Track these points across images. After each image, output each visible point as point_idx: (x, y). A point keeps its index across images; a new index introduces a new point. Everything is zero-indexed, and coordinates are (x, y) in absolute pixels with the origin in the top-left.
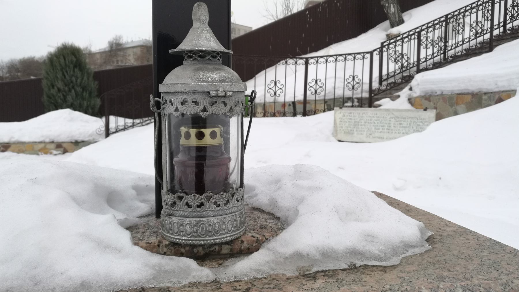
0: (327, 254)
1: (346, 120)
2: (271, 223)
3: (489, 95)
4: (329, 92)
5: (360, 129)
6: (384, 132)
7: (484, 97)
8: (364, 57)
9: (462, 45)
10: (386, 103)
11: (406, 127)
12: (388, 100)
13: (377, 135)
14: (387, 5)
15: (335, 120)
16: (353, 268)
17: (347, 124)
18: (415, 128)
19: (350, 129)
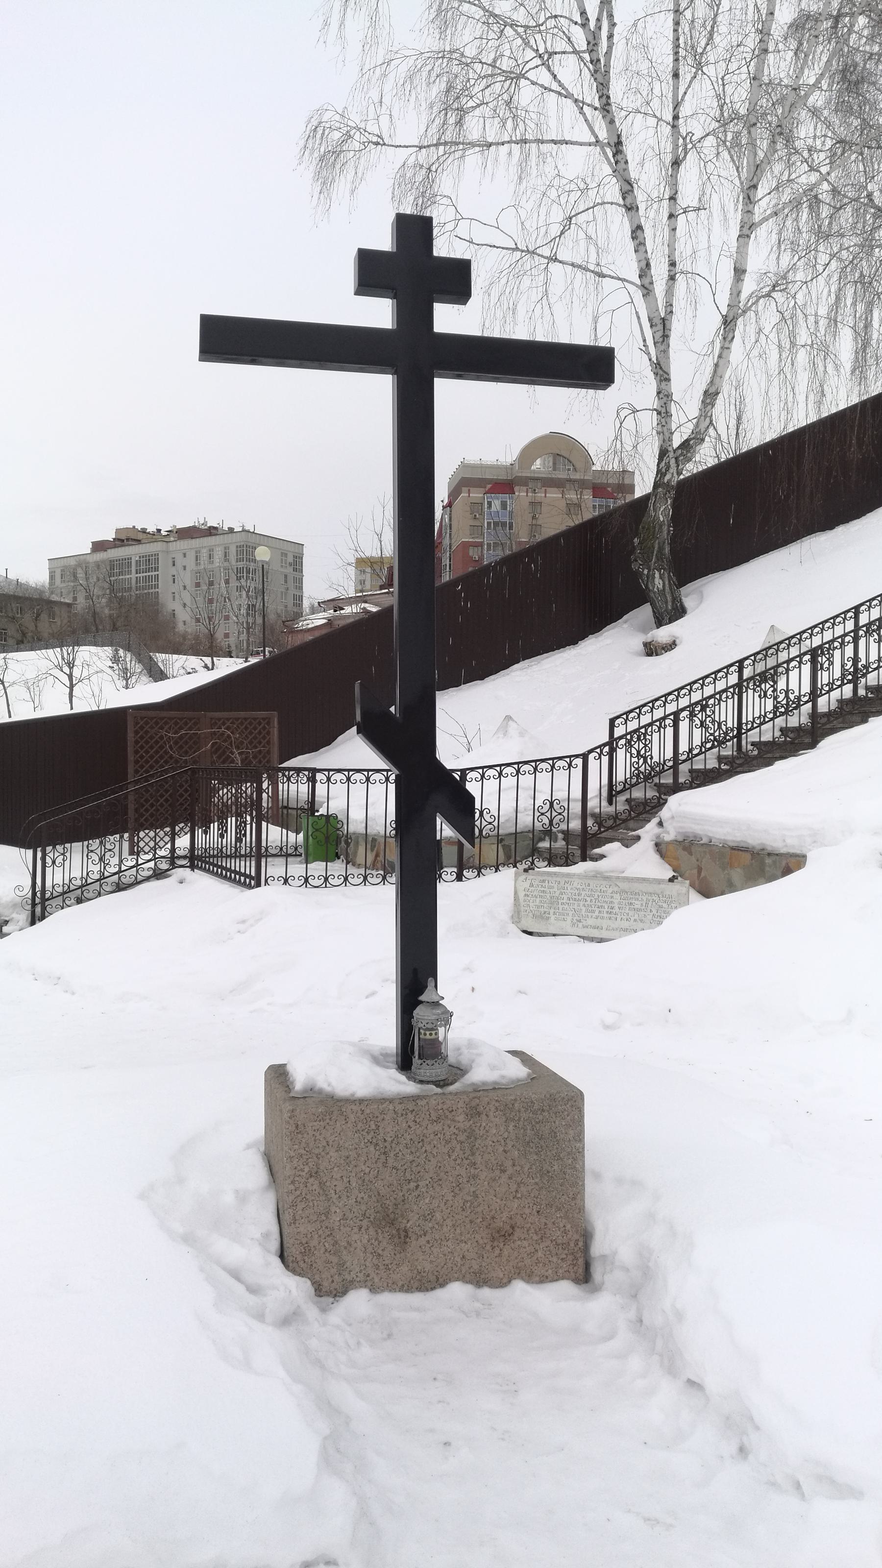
0: (484, 1083)
1: (535, 893)
2: (459, 1072)
3: (774, 858)
4: (507, 821)
5: (560, 910)
6: (603, 918)
7: (768, 861)
8: (570, 765)
9: (772, 719)
10: (613, 849)
11: (640, 910)
12: (616, 845)
13: (590, 922)
14: (646, 572)
15: (516, 893)
16: (494, 1089)
17: (538, 900)
18: (654, 912)
19: (542, 910)
